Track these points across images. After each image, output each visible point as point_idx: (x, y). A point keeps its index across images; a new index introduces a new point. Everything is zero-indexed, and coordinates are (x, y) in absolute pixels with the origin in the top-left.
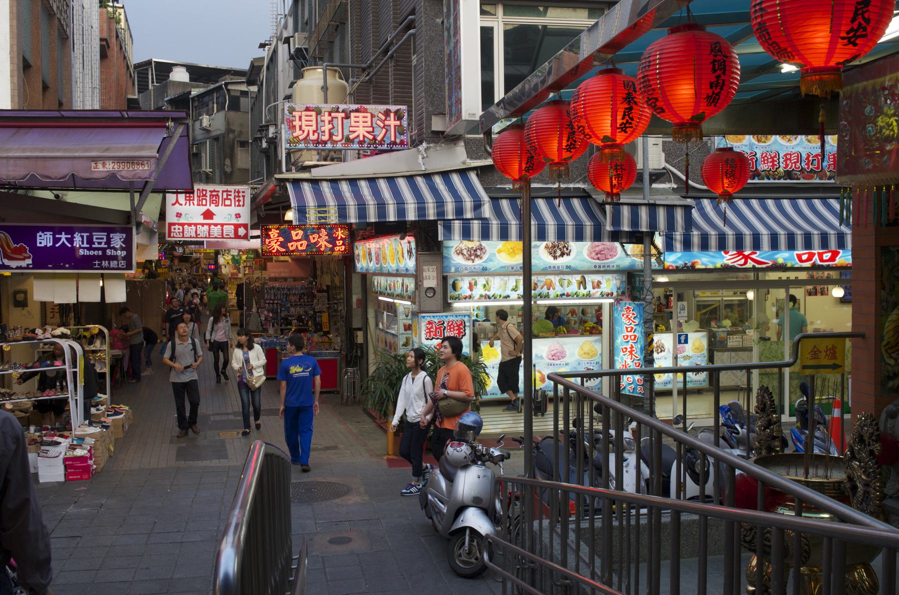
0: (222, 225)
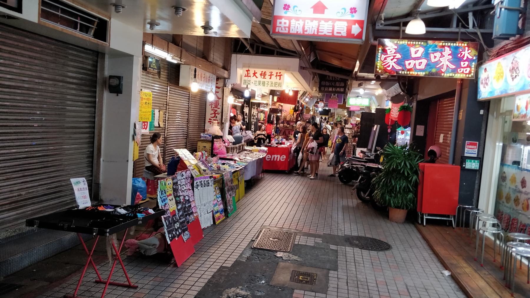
0: (334, 21)
